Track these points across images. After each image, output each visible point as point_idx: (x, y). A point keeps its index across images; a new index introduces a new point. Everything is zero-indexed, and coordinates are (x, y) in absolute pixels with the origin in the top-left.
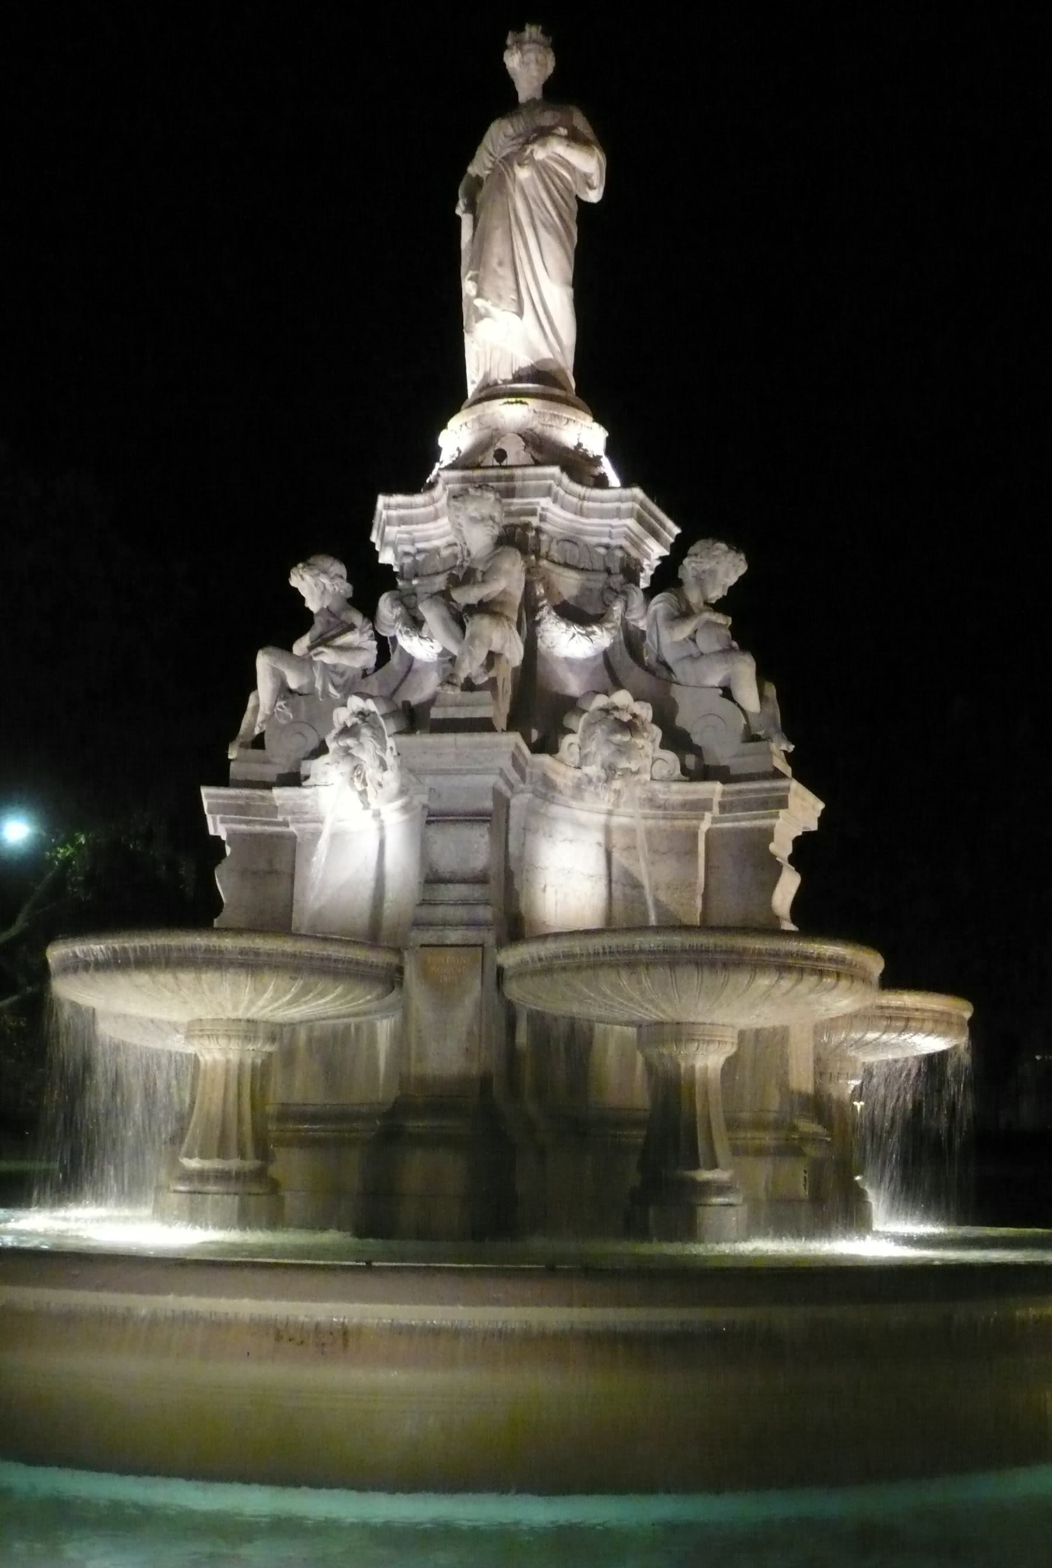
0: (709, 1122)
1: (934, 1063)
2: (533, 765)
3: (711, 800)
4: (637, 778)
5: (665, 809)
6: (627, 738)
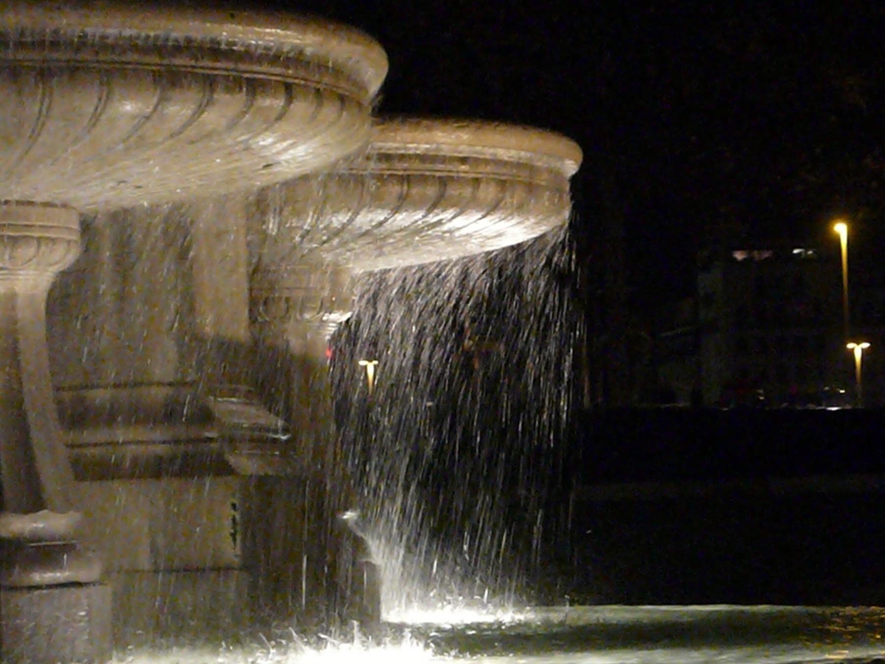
0: (22, 416)
1: (506, 266)
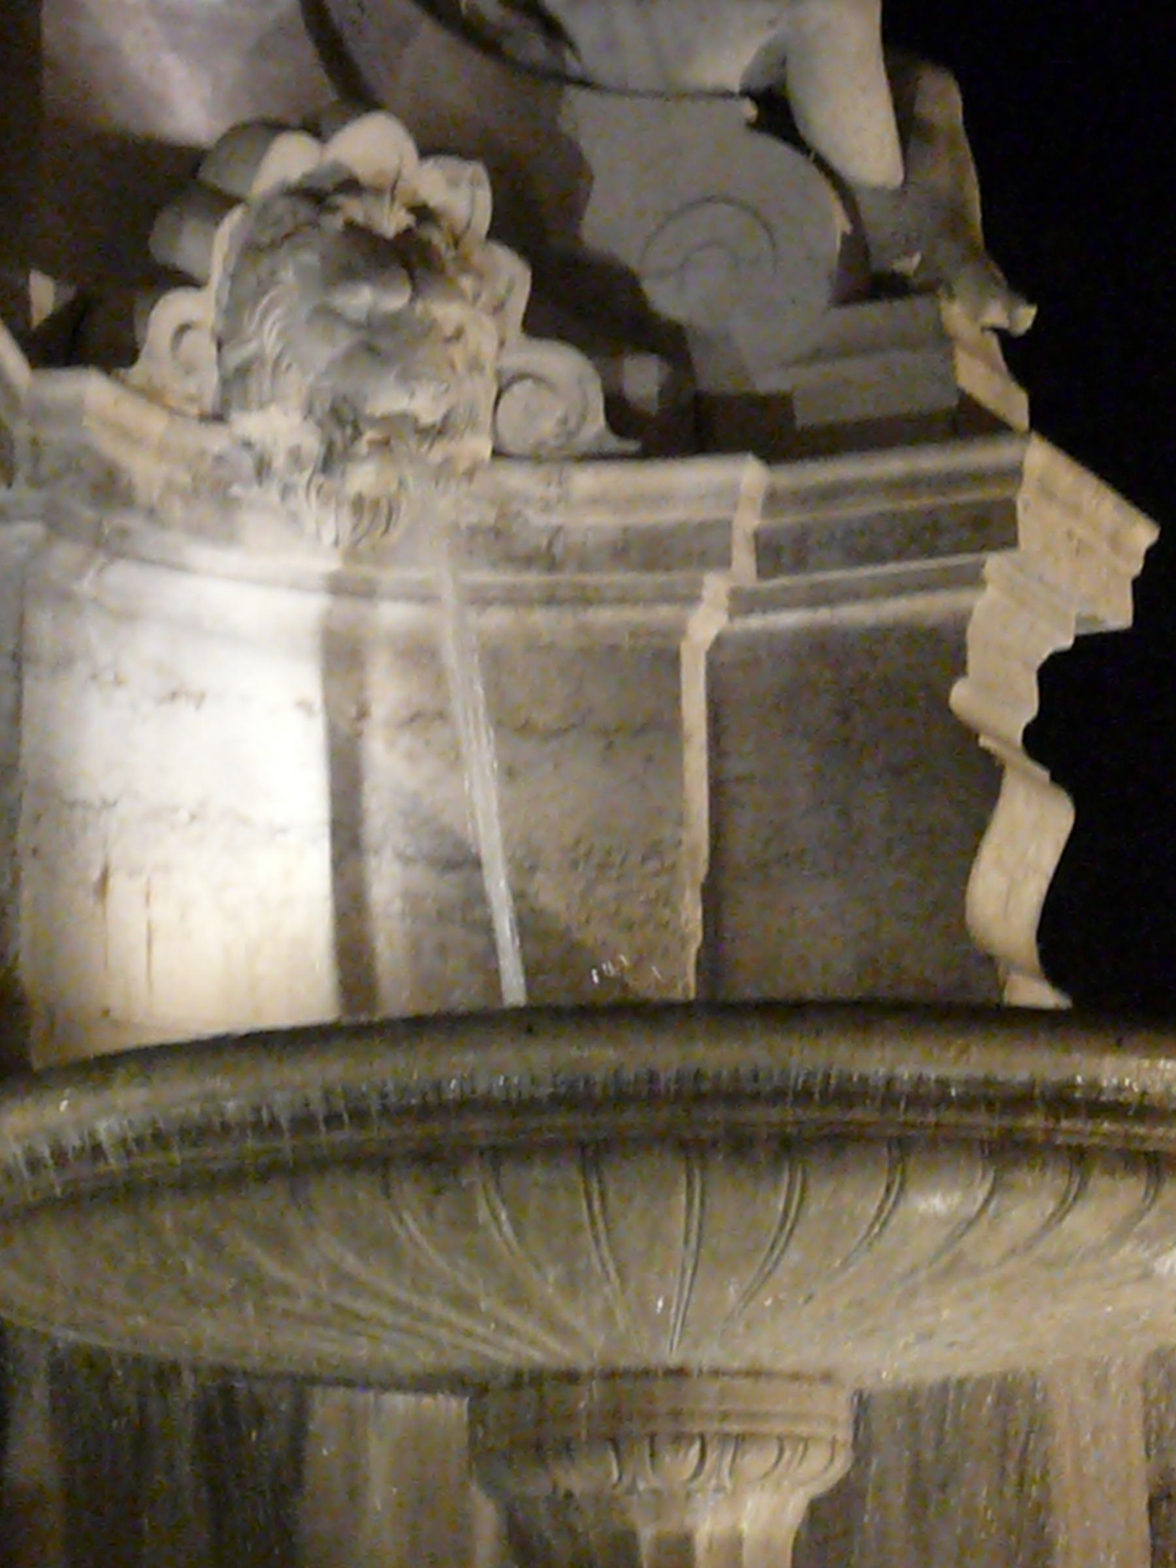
2: (41, 413)
3: (726, 526)
4: (437, 454)
5: (552, 564)
6: (395, 300)
